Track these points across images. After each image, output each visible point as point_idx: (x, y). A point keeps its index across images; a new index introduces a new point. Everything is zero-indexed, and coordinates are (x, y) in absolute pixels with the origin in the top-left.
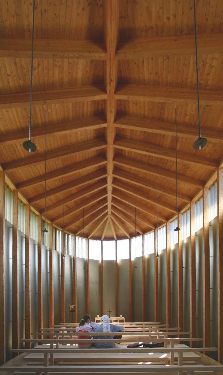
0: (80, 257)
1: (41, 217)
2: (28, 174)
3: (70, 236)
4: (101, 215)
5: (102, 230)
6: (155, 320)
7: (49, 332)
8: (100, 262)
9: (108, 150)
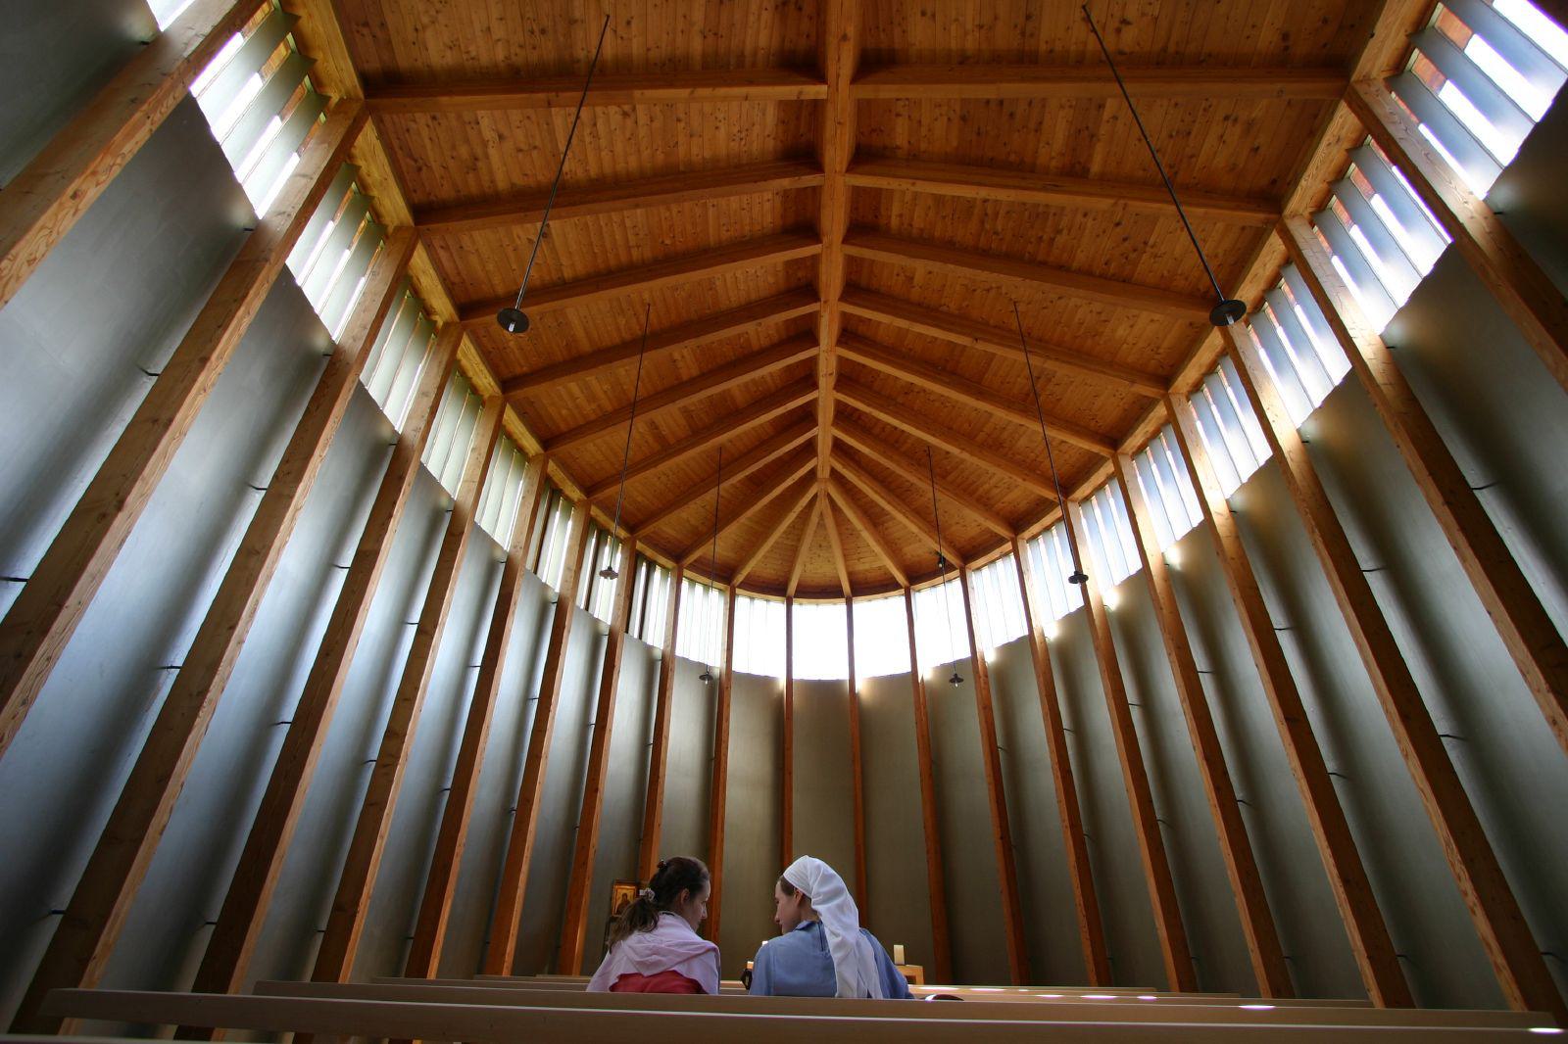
0: (694, 657)
2: (514, 267)
4: (789, 482)
5: (790, 554)
8: (782, 684)
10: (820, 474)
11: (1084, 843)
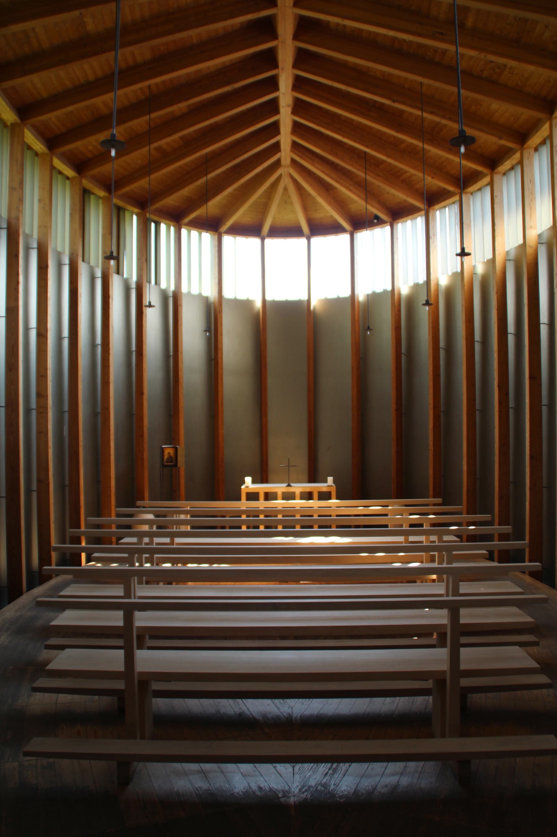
0: (195, 291)
1: (81, 183)
3: (163, 227)
6: (431, 493)
7: (99, 526)
8: (258, 304)
9: (280, 19)
10: (283, 162)
11: (439, 417)
